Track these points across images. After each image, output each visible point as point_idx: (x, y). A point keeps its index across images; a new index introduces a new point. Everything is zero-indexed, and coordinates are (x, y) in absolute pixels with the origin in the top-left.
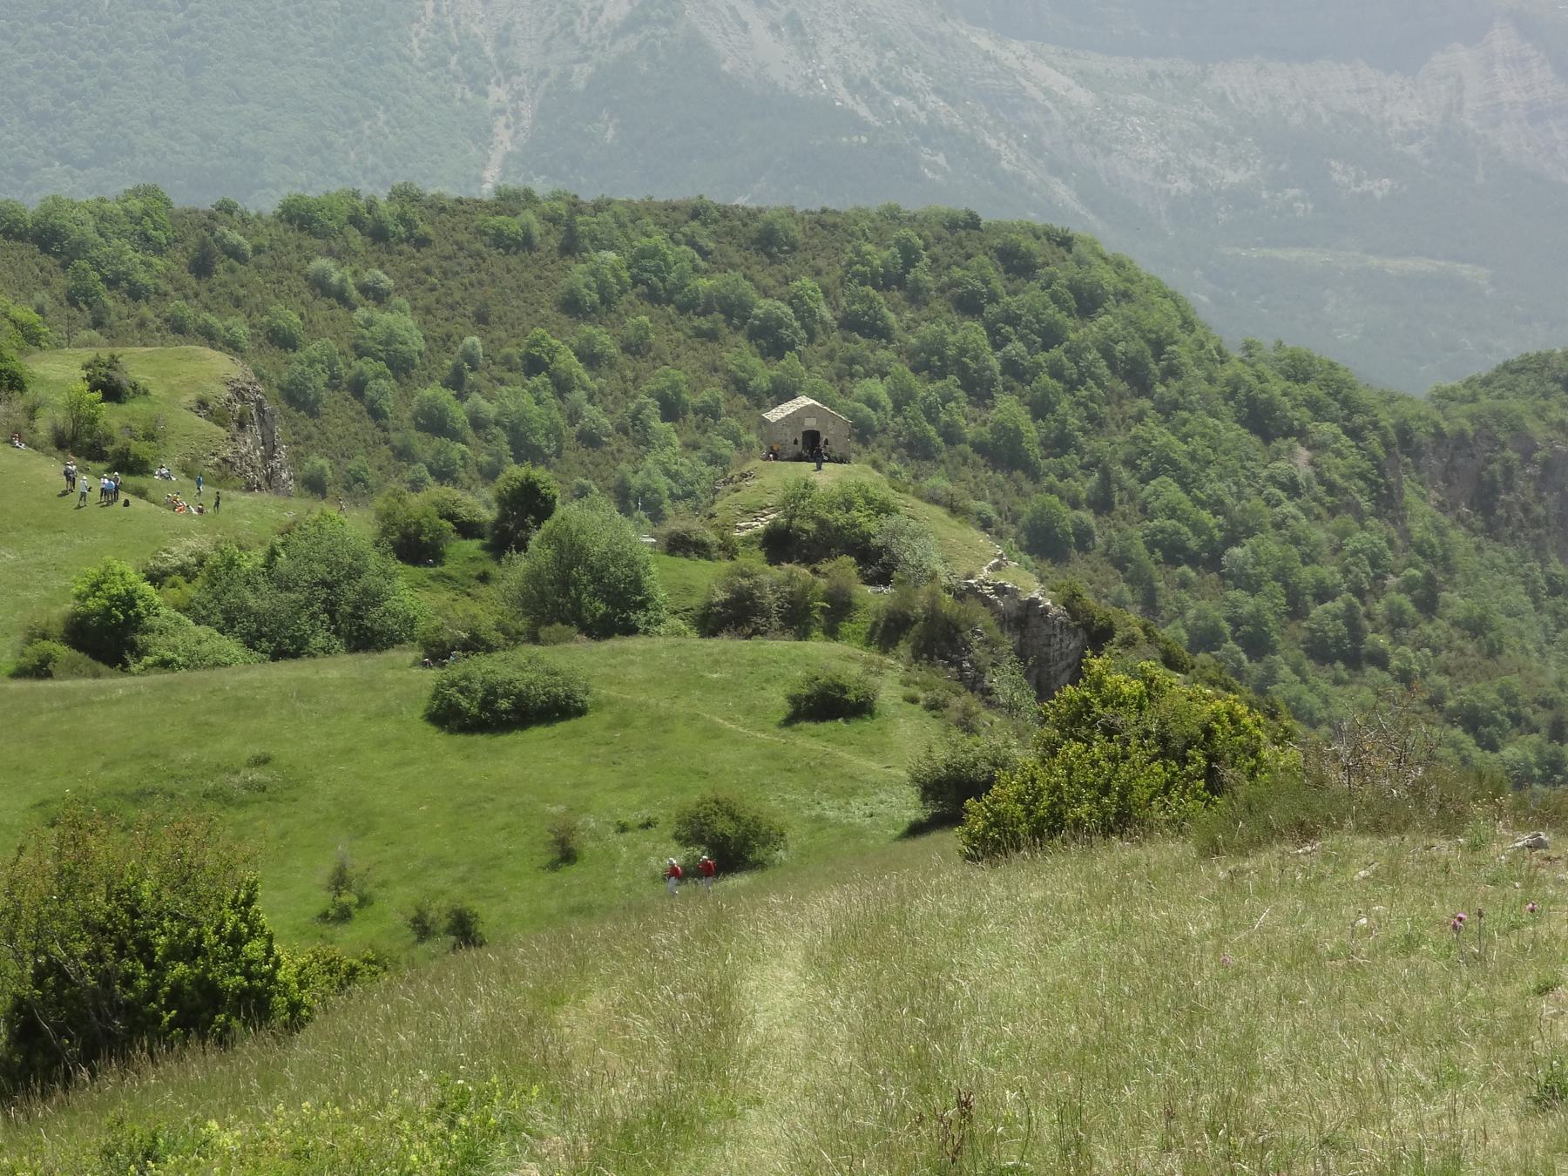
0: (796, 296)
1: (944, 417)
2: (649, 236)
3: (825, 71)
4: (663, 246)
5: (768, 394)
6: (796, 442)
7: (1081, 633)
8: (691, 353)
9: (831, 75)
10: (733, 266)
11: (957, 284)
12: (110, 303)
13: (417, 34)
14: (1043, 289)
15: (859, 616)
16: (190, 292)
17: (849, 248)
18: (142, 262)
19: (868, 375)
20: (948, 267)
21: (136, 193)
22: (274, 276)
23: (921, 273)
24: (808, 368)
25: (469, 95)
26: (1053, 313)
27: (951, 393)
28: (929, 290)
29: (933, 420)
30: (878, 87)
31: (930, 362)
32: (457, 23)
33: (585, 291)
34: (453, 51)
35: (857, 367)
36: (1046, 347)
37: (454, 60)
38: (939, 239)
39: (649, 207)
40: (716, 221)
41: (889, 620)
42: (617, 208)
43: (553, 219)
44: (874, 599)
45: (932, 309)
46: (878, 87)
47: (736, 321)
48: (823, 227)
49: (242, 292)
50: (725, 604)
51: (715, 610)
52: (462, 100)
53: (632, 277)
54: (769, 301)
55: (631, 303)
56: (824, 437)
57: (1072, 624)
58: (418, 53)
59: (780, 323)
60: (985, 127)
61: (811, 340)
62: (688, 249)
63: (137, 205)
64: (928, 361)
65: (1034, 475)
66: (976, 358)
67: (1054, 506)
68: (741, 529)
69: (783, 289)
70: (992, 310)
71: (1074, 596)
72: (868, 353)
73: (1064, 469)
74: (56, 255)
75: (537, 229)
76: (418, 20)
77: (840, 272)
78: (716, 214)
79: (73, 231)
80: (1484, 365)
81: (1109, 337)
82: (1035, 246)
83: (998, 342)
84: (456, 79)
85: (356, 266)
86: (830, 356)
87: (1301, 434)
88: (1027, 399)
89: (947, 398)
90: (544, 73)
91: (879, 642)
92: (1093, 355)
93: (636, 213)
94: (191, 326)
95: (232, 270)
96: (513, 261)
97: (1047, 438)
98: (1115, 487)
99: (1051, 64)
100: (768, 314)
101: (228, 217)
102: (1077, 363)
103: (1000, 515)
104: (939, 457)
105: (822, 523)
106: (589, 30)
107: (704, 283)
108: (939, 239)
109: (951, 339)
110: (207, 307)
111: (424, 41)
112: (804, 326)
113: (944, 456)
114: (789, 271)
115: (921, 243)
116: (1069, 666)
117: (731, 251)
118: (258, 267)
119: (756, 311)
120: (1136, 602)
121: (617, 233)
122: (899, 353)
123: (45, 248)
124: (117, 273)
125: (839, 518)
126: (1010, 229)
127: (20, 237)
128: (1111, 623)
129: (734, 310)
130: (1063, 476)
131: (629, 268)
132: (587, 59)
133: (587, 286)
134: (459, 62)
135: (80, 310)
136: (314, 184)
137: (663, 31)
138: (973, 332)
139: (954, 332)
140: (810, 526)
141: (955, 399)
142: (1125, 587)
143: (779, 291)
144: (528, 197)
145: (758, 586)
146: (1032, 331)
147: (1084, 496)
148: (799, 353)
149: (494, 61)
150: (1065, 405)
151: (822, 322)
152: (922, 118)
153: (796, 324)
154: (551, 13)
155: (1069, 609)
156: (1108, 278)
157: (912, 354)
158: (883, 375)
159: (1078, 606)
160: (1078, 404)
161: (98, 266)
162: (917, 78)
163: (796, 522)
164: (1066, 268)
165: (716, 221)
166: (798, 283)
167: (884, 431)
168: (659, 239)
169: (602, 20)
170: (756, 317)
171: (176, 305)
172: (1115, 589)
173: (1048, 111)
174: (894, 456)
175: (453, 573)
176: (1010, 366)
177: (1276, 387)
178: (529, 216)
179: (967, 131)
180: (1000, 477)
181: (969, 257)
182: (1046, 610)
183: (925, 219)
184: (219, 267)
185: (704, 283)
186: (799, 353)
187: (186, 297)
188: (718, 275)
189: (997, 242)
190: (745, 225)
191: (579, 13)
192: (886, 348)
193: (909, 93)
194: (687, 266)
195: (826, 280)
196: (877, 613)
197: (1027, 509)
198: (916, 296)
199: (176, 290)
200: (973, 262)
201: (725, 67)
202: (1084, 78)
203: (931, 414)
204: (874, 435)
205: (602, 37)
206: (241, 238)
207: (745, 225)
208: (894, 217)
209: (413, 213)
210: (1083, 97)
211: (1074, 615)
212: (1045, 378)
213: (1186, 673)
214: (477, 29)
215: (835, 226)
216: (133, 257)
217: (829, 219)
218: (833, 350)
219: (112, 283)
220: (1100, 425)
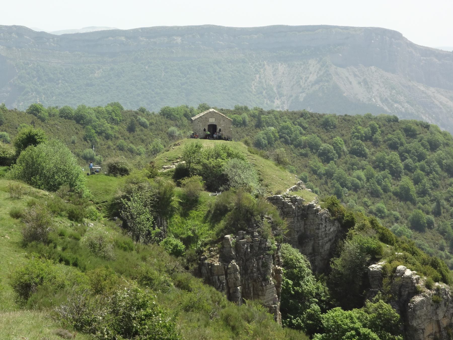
0: (335, 143)
1: (383, 183)
2: (286, 122)
3: (374, 96)
4: (290, 125)
5: (324, 175)
6: (205, 130)
7: (337, 223)
8: (298, 161)
9: (376, 97)
10: (314, 132)
11: (390, 139)
12: (98, 140)
13: (254, 84)
14: (419, 142)
16: (126, 138)
17: (353, 127)
18: (110, 127)
19: (358, 169)
20: (387, 134)
21: (112, 105)
22: (156, 133)
23: (378, 136)
24: (338, 167)
25: (269, 102)
26: (421, 149)
27: (386, 176)
28: (380, 142)
29: (379, 184)
30: (390, 101)
31: (379, 165)
32: (266, 81)
33: (263, 140)
34: (264, 90)
35: (355, 166)
36: (419, 161)
37: (264, 92)
38: (384, 125)
39: (287, 113)
40: (309, 118)
41: (216, 210)
42: (275, 113)
43: (253, 116)
45: (381, 148)
46: (390, 101)
47: (314, 151)
48: (345, 120)
49: (145, 138)
52: (267, 104)
53: (279, 136)
54: (325, 144)
55: (279, 144)
56: (218, 128)
57: (332, 218)
58: (254, 90)
59: (329, 151)
60: (422, 113)
61: (340, 157)
62: (299, 127)
63: (110, 108)
64: (379, 165)
65: (414, 203)
66: (395, 164)
67: (420, 213)
68: (165, 168)
69: (331, 140)
70: (401, 148)
71: (333, 204)
72: (359, 162)
73: (424, 201)
74: (82, 124)
75: (247, 119)
76: (254, 80)
77: (350, 135)
78: (309, 116)
79: (87, 116)
81: (441, 158)
82: (416, 128)
83: (403, 159)
84: (265, 98)
85: (185, 130)
86: (346, 163)
88: (412, 178)
89: (384, 177)
90: (291, 96)
91: (210, 222)
92: (435, 163)
93: (282, 114)
94: (126, 149)
95: (142, 130)
96: (239, 129)
97: (419, 191)
98: (442, 208)
99: (442, 95)
100: (325, 149)
101: (142, 113)
102: (429, 166)
103: (402, 216)
104: (381, 197)
105: (204, 165)
106: (304, 84)
107: (304, 138)
108: (384, 125)
109: (387, 157)
110: (132, 142)
111: (256, 86)
112: (337, 153)
113: (384, 196)
114: (333, 135)
115: (378, 126)
116: (330, 240)
117: (313, 128)
118: (151, 130)
119: (321, 147)
120: (448, 246)
121: (275, 121)
122: (369, 162)
123: (78, 122)
124: (101, 130)
125: (212, 162)
126: (409, 122)
127: (70, 118)
128: (353, 219)
129: (313, 147)
130: (423, 204)
131: (278, 132)
132: (304, 92)
133: (263, 138)
134: (266, 93)
135: (88, 142)
136: (174, 103)
137: (326, 84)
138: (394, 155)
139: (388, 155)
141: (388, 178)
142: (444, 241)
143: (329, 141)
144: (246, 109)
146: (415, 155)
147: (431, 210)
148: (335, 162)
149: (276, 93)
150: (425, 180)
151: (343, 151)
152: (403, 110)
153: (335, 152)
154: (293, 78)
156: (441, 138)
157: (374, 162)
158: (363, 169)
159: (335, 209)
160: (430, 180)
161: (94, 127)
162: (402, 98)
164: (427, 135)
165: (309, 118)
166: (336, 139)
167: (363, 188)
168: (289, 123)
169: (308, 81)
170: (321, 149)
171: (121, 141)
172: (441, 242)
173: (441, 108)
174: (366, 196)
176: (407, 167)
178: (245, 115)
179: (417, 114)
180: (402, 203)
181: (394, 131)
182: (317, 211)
183: (380, 118)
184: (137, 129)
185: (304, 138)
186: (335, 162)
187: (125, 139)
188: (309, 135)
189: (404, 126)
190: (319, 119)
191: (302, 78)
192: (365, 160)
193: (400, 103)
194: (298, 132)
195: (345, 138)
197: (411, 215)
198: (376, 143)
199: (122, 136)
200: (395, 133)
201: (345, 95)
203: (379, 183)
204: (360, 189)
205: (308, 86)
206: (146, 120)
207: (319, 119)
208: (369, 118)
211: (333, 214)
212: (419, 171)
213: (392, 245)
214: (272, 83)
215: (349, 120)
216: (108, 125)
217: (347, 118)
218: (347, 161)
219: (99, 134)
220: (437, 187)
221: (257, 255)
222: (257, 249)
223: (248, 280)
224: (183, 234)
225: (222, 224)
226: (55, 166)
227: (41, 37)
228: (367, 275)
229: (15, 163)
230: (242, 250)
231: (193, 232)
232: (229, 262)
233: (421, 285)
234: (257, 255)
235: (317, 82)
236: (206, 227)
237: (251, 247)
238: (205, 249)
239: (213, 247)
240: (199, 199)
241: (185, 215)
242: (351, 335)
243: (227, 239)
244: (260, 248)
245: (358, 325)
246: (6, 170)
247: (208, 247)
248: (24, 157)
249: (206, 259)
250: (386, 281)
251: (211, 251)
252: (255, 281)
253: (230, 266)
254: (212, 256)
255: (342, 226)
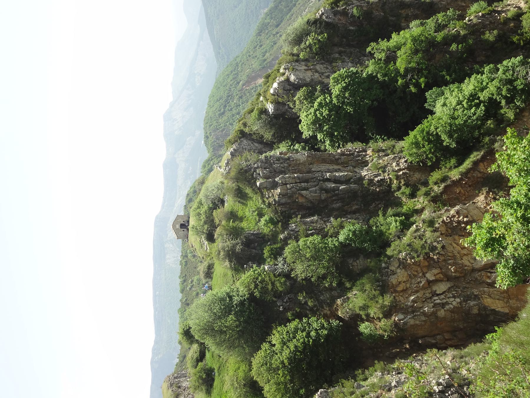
15: (236, 208)
39: (182, 246)
41: (237, 197)
43: (183, 258)
44: (230, 203)
50: (230, 261)
51: (233, 266)
56: (182, 222)
57: (239, 142)
63: (180, 313)
80: (206, 148)
87: (212, 166)
91: (246, 200)
105: (205, 223)
116: (252, 143)
136: (178, 288)
140: (206, 227)
145: (223, 249)
155: (234, 143)
156: (192, 190)
159: (233, 140)
163: (205, 231)
175: (218, 365)
177: (206, 169)
182: (234, 150)
196: (235, 201)
202: (179, 198)
209: (182, 276)
210: (181, 198)
221: (271, 165)
222: (267, 165)
223: (289, 170)
224: (255, 219)
225: (248, 191)
226: (207, 312)
227: (156, 342)
228: (276, 116)
229: (204, 343)
230: (268, 174)
231: (254, 212)
232: (277, 183)
233: (282, 79)
234: (271, 165)
235: (173, 244)
236: (250, 203)
237: (265, 168)
238: (267, 202)
239: (265, 195)
240: (230, 211)
241: (241, 219)
242: (319, 113)
243: (261, 184)
244: (266, 163)
245: (312, 110)
246: (209, 351)
247: (265, 199)
248: (199, 336)
249: (275, 200)
250: (280, 100)
251: (269, 197)
252: (290, 165)
253: (280, 182)
254: (273, 195)
255: (243, 137)
